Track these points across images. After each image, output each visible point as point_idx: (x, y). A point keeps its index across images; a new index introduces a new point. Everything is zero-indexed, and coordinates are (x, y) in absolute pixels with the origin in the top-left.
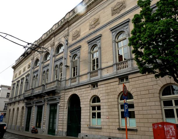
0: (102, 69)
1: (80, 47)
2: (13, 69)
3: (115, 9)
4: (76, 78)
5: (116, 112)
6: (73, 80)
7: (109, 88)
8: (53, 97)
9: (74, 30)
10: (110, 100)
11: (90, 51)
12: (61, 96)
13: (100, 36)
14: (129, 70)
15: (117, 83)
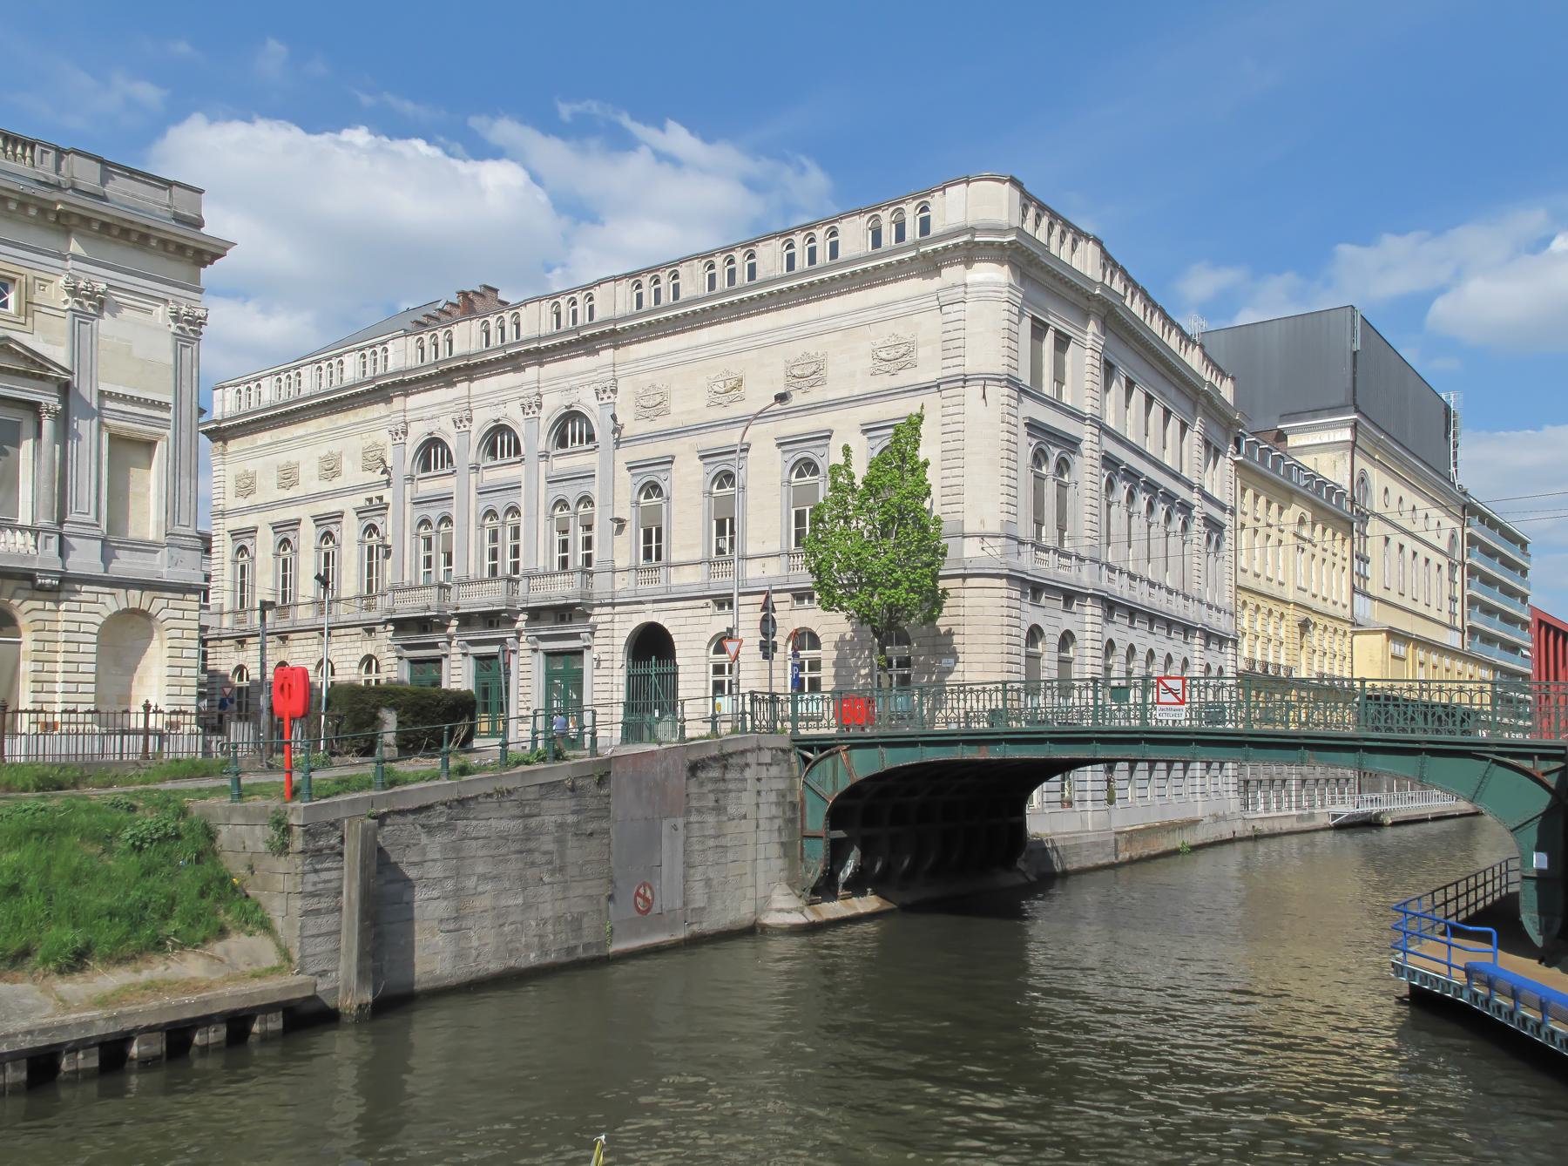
0: (745, 558)
1: (671, 462)
2: (976, 266)
4: (245, 612)
5: (142, 717)
6: (645, 576)
9: (642, 377)
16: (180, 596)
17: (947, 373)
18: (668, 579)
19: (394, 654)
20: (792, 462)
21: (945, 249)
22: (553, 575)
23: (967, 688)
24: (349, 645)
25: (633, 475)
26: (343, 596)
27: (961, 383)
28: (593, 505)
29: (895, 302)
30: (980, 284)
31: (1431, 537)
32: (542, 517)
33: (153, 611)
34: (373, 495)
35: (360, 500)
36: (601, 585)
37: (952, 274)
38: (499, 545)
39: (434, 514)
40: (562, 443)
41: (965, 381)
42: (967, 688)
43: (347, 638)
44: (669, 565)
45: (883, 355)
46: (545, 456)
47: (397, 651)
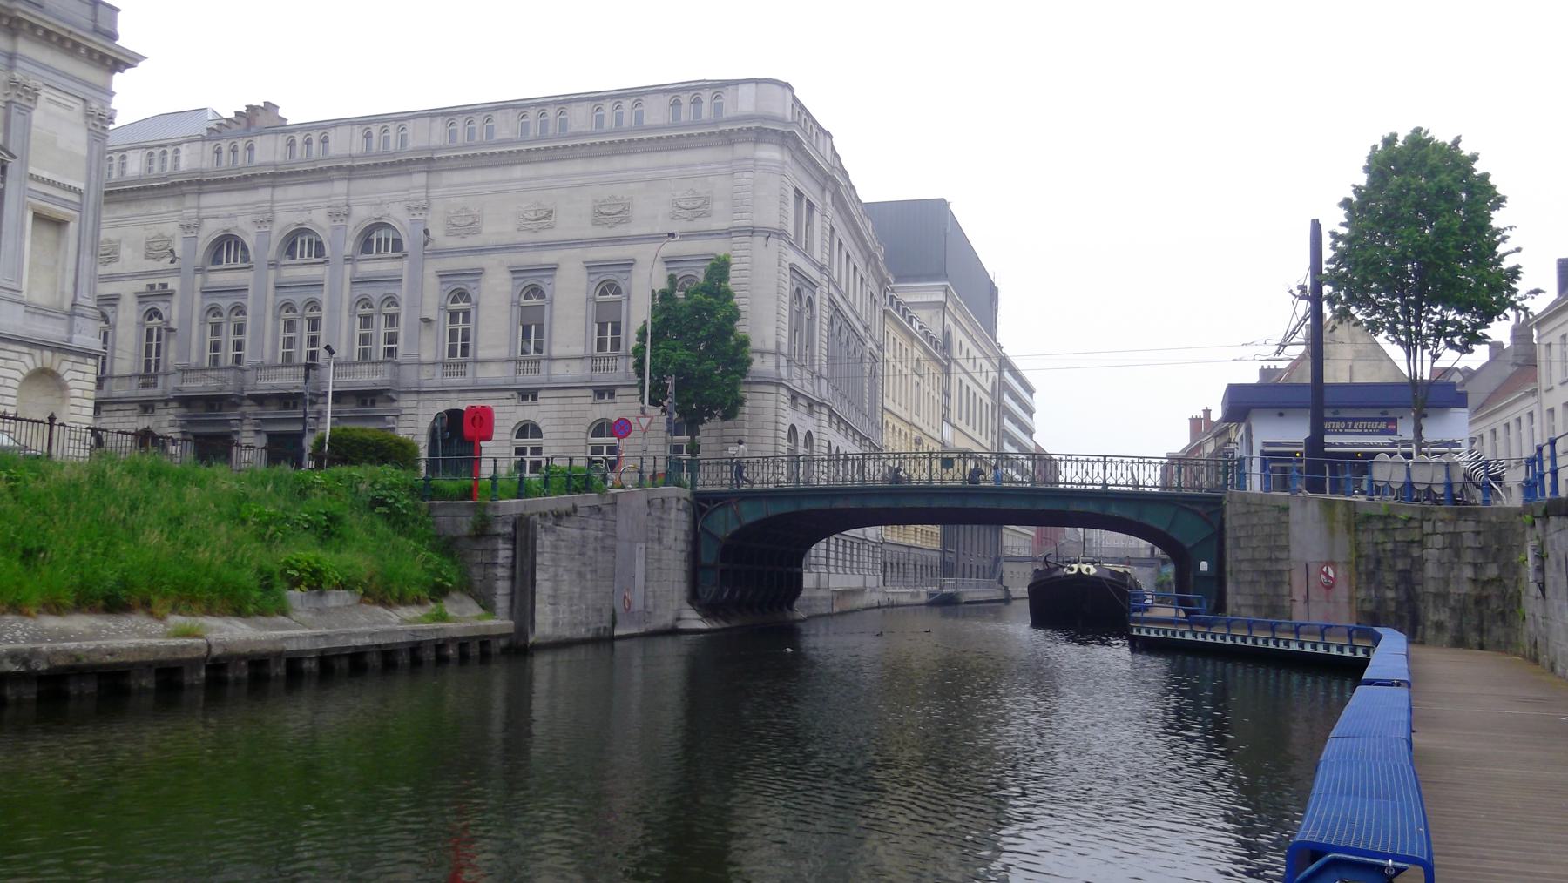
3: (602, 210)
7: (568, 408)
8: (368, 412)
10: (567, 436)
11: (516, 298)
12: (404, 411)
13: (553, 268)
14: (618, 379)
15: (590, 400)
16: (81, 359)
17: (736, 223)
18: (474, 373)
19: (178, 430)
20: (449, 291)
21: (740, 130)
22: (354, 364)
23: (1074, 458)
24: (122, 420)
25: (442, 283)
26: (116, 374)
27: (749, 233)
28: (245, 314)
29: (693, 165)
30: (767, 160)
31: (982, 380)
32: (345, 314)
33: (61, 372)
34: (157, 281)
35: (141, 285)
36: (410, 377)
37: (743, 150)
38: (221, 339)
39: (225, 303)
40: (216, 259)
41: (753, 232)
42: (1074, 458)
43: (120, 413)
44: (476, 361)
45: (683, 204)
46: (274, 265)
47: (182, 426)
